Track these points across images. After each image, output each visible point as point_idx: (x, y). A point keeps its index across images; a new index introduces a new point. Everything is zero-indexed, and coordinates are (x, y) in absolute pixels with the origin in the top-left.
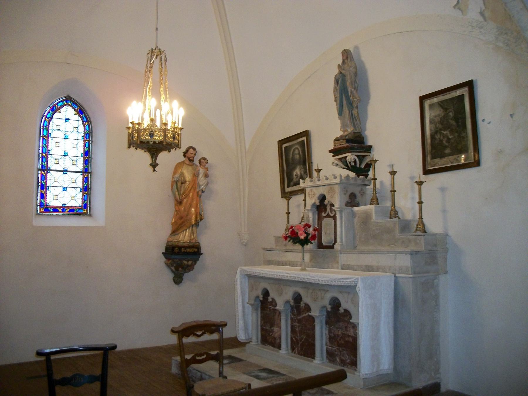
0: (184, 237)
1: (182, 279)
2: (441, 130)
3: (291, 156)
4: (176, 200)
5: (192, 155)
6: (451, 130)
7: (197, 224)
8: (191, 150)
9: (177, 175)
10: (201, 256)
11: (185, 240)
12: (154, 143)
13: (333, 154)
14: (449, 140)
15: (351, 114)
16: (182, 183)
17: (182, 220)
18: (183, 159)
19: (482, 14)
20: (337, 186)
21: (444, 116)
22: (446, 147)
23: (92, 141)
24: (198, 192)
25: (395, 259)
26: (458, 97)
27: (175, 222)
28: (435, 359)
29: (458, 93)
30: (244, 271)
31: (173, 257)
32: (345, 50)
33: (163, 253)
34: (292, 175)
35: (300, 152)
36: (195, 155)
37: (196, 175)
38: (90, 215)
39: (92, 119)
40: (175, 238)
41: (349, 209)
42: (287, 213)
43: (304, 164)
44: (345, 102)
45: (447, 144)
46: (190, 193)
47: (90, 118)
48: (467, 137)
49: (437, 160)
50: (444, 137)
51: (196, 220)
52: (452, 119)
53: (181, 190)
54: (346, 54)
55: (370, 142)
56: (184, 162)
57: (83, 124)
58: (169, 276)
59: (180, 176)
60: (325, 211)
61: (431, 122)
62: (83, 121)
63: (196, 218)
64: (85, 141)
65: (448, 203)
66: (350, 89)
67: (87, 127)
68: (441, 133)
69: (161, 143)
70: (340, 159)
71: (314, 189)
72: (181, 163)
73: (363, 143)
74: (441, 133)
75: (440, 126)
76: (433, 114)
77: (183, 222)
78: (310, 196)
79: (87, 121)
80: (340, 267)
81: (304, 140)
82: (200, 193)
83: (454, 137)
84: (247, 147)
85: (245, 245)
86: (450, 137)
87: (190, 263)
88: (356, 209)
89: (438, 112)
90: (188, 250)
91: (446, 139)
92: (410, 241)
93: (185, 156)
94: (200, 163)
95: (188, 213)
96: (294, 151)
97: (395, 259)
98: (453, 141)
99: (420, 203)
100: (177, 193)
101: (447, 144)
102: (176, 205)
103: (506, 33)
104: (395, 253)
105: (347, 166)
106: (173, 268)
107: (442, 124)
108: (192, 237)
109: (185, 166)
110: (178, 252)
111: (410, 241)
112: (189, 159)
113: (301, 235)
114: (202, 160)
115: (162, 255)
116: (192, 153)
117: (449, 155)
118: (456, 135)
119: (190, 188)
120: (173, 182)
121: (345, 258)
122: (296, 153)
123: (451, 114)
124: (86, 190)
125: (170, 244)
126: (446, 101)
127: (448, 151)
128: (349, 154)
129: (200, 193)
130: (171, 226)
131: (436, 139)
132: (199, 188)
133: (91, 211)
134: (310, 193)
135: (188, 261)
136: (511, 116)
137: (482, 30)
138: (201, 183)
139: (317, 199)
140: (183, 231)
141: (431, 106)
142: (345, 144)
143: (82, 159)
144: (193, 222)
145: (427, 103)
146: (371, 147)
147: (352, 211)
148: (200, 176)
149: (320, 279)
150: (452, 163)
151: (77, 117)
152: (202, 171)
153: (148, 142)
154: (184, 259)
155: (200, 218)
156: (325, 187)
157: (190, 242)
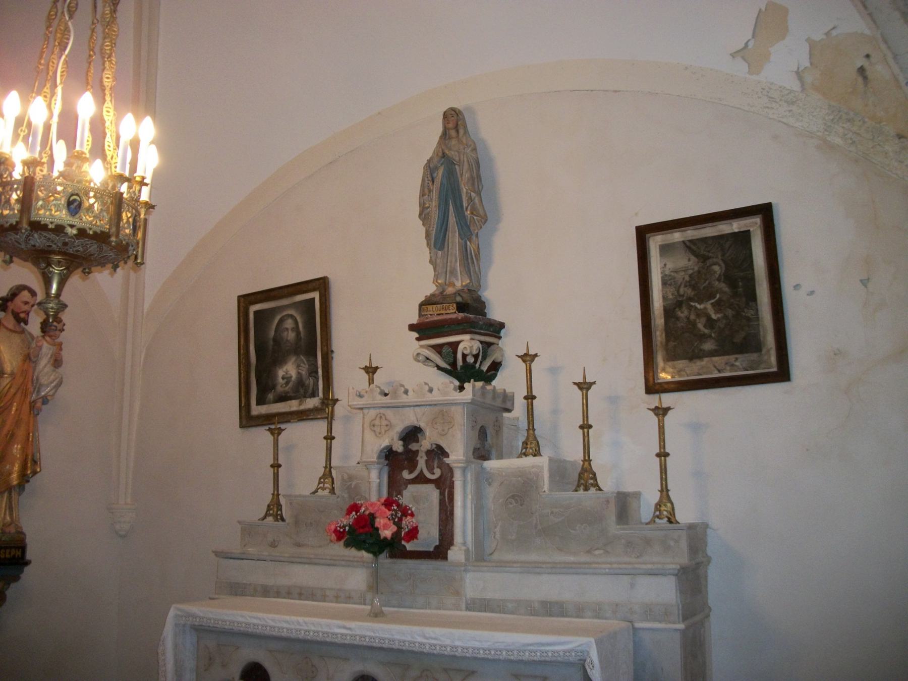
2: (690, 299)
3: (272, 333)
5: (26, 308)
6: (716, 303)
7: (21, 487)
8: (25, 295)
10: (27, 569)
12: (82, 233)
13: (417, 335)
14: (710, 323)
15: (464, 250)
19: (799, 74)
20: (459, 409)
21: (699, 272)
22: (703, 337)
24: (35, 402)
25: (632, 586)
26: (734, 234)
29: (736, 226)
30: (189, 615)
32: (453, 109)
34: (276, 376)
37: (29, 359)
41: (475, 465)
43: (310, 352)
44: (452, 219)
45: (706, 331)
46: (11, 404)
48: (758, 319)
50: (698, 315)
52: (719, 280)
54: (454, 122)
55: (495, 313)
60: (412, 466)
61: (664, 283)
63: (24, 467)
65: (728, 456)
66: (456, 197)
68: (690, 308)
69: (101, 237)
70: (438, 348)
71: (389, 413)
73: (485, 315)
74: (690, 308)
75: (690, 292)
76: (670, 266)
78: (377, 429)
80: (463, 606)
81: (313, 299)
82: (39, 404)
83: (726, 317)
85: (123, 537)
86: (714, 317)
88: (492, 465)
89: (683, 262)
91: (703, 320)
92: (648, 542)
96: (281, 321)
97: (632, 586)
98: (722, 326)
101: (706, 331)
103: (849, 120)
104: (633, 574)
105: (454, 364)
107: (694, 287)
108: (8, 518)
111: (648, 542)
113: (386, 527)
116: (26, 303)
118: (730, 312)
119: (13, 391)
121: (475, 583)
122: (290, 328)
123: (716, 268)
126: (704, 240)
127: (708, 346)
128: (466, 337)
131: (678, 319)
132: (39, 392)
134: (377, 422)
136: (865, 282)
137: (794, 108)
138: (44, 380)
139: (396, 437)
141: (665, 249)
142: (451, 313)
144: (14, 479)
145: (655, 243)
146: (502, 326)
147: (483, 469)
149: (457, 643)
152: (47, 349)
153: (60, 229)
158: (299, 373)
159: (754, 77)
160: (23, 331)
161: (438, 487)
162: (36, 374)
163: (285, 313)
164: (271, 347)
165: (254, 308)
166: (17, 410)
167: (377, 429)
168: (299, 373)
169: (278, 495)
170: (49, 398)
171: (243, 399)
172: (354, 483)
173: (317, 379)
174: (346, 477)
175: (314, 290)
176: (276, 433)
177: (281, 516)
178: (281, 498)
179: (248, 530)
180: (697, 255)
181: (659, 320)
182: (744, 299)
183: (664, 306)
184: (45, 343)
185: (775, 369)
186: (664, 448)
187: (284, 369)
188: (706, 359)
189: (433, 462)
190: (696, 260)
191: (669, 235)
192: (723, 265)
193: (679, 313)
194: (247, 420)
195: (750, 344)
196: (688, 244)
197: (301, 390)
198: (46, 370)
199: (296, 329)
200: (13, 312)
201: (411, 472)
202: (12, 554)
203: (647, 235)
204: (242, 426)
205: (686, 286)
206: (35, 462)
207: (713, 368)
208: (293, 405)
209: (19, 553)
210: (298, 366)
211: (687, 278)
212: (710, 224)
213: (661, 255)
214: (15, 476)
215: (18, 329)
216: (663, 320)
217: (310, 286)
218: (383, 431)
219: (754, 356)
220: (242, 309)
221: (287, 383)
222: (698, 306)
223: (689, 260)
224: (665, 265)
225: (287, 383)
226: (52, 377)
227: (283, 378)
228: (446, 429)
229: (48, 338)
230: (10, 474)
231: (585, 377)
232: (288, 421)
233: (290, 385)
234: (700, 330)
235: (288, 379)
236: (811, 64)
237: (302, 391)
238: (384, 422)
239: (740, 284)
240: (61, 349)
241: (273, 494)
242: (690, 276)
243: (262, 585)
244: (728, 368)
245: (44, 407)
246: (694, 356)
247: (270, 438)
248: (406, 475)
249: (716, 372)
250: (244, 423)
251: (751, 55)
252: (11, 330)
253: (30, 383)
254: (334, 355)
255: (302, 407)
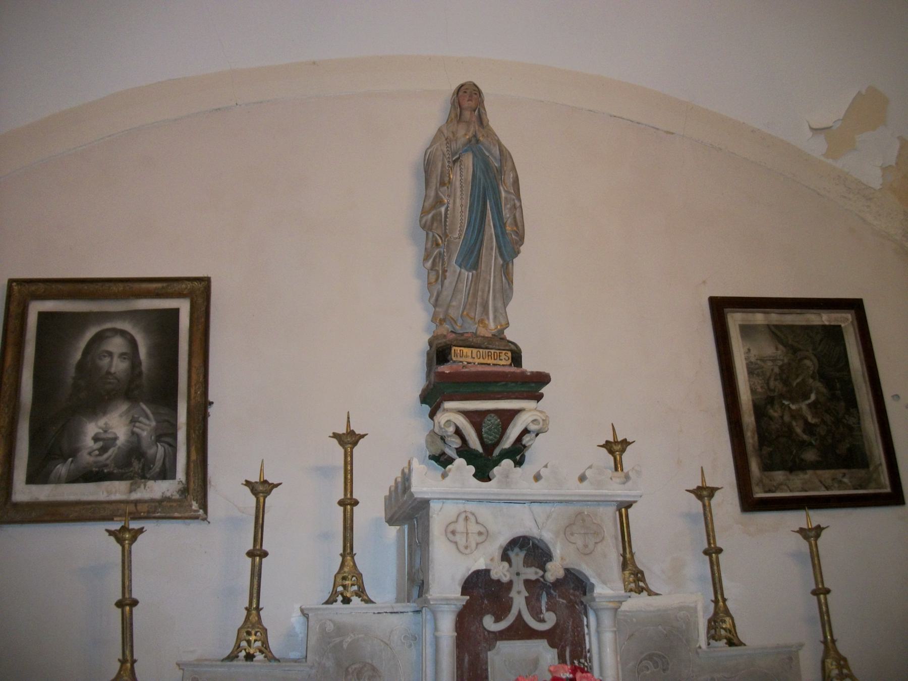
2: (782, 396)
14: (809, 428)
21: (789, 364)
22: (803, 445)
43: (164, 396)
44: (490, 229)
45: (805, 437)
49: (779, 476)
50: (793, 417)
52: (813, 377)
60: (501, 609)
61: (751, 372)
66: (472, 203)
71: (484, 512)
76: (754, 352)
89: (768, 349)
96: (99, 338)
98: (823, 433)
99: (257, 553)
101: (805, 437)
107: (786, 382)
117: (815, 466)
118: (828, 418)
123: (808, 362)
126: (792, 328)
127: (810, 456)
134: (460, 527)
145: (845, 320)
150: (827, 488)
156: (547, 508)
158: (133, 433)
159: (830, 161)
161: (552, 645)
163: (108, 325)
164: (70, 381)
165: (36, 308)
167: (461, 539)
168: (133, 433)
171: (870, 426)
172: (349, 639)
173: (174, 447)
174: (330, 627)
175: (179, 295)
176: (125, 538)
180: (785, 345)
181: (748, 419)
182: (843, 404)
183: (753, 401)
185: (888, 490)
187: (102, 422)
188: (810, 472)
189: (539, 600)
190: (784, 349)
191: (750, 315)
192: (815, 361)
193: (771, 412)
195: (855, 459)
196: (773, 328)
197: (133, 464)
201: (498, 620)
203: (726, 310)
205: (776, 380)
207: (819, 484)
210: (133, 421)
211: (777, 370)
212: (799, 311)
213: (742, 337)
216: (753, 418)
217: (177, 287)
218: (474, 545)
219: (862, 473)
221: (103, 450)
222: (793, 407)
223: (777, 349)
224: (749, 350)
225: (103, 450)
227: (96, 439)
228: (591, 546)
231: (703, 480)
234: (797, 435)
235: (105, 442)
236: (897, 164)
237: (137, 466)
238: (473, 528)
239: (838, 385)
242: (781, 367)
244: (836, 485)
246: (795, 466)
248: (489, 623)
249: (823, 488)
251: (838, 138)
254: (420, 393)
255: (135, 496)
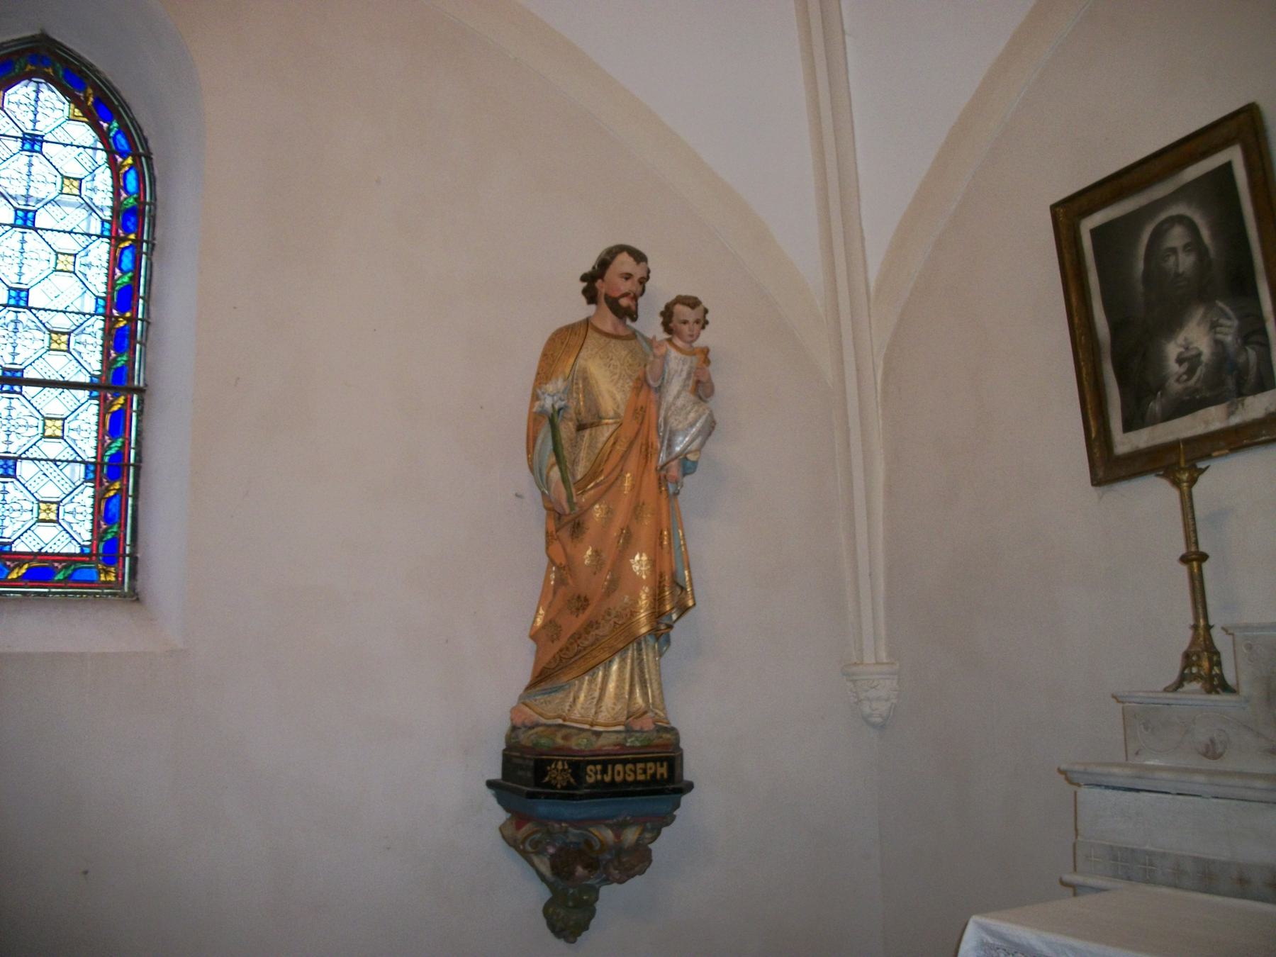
0: (600, 702)
1: (592, 913)
3: (1140, 266)
4: (554, 513)
5: (626, 286)
7: (661, 631)
8: (624, 263)
9: (556, 385)
10: (685, 799)
11: (602, 717)
16: (581, 427)
17: (583, 617)
18: (580, 310)
23: (152, 246)
27: (550, 623)
28: (626, 598)
31: (543, 808)
33: (491, 784)
35: (1205, 234)
36: (643, 281)
37: (646, 386)
38: (134, 596)
39: (152, 144)
40: (551, 707)
42: (1184, 559)
47: (144, 141)
51: (657, 614)
53: (574, 463)
56: (587, 323)
57: (112, 163)
58: (522, 890)
59: (568, 391)
62: (112, 153)
63: (657, 599)
64: (115, 240)
67: (131, 178)
72: (570, 330)
77: (591, 625)
79: (132, 151)
81: (1228, 167)
82: (674, 469)
84: (872, 284)
87: (631, 835)
90: (620, 773)
93: (591, 295)
94: (667, 315)
95: (618, 575)
96: (1158, 235)
100: (555, 473)
102: (550, 538)
106: (545, 869)
108: (639, 700)
109: (593, 338)
110: (569, 786)
112: (613, 305)
114: (681, 310)
115: (490, 798)
116: (628, 277)
119: (620, 448)
120: (536, 418)
124: (113, 471)
125: (525, 738)
129: (674, 469)
130: (531, 645)
132: (670, 446)
133: (140, 576)
135: (619, 828)
140: (592, 669)
143: (99, 323)
148: (674, 387)
151: (84, 133)
152: (678, 364)
154: (597, 821)
155: (672, 598)
157: (629, 731)
160: (634, 335)
162: (662, 413)
163: (1163, 216)
166: (633, 486)
169: (1208, 628)
170: (691, 457)
171: (1074, 300)
177: (1221, 677)
178: (1217, 635)
179: (1139, 717)
184: (673, 353)
186: (1196, 543)
187: (1180, 339)
194: (1108, 467)
198: (680, 402)
199: (1195, 243)
200: (607, 298)
202: (650, 772)
204: (1097, 481)
206: (679, 586)
208: (1213, 419)
209: (663, 770)
210: (1214, 326)
214: (643, 615)
215: (621, 331)
220: (1068, 265)
221: (1191, 372)
226: (692, 415)
227: (1180, 361)
229: (679, 343)
230: (633, 613)
232: (1208, 456)
233: (1200, 371)
235: (1190, 361)
240: (707, 361)
241: (1195, 627)
243: (1196, 860)
245: (687, 479)
247: (1174, 494)
250: (1101, 474)
252: (607, 335)
253: (653, 432)
255: (1235, 420)
